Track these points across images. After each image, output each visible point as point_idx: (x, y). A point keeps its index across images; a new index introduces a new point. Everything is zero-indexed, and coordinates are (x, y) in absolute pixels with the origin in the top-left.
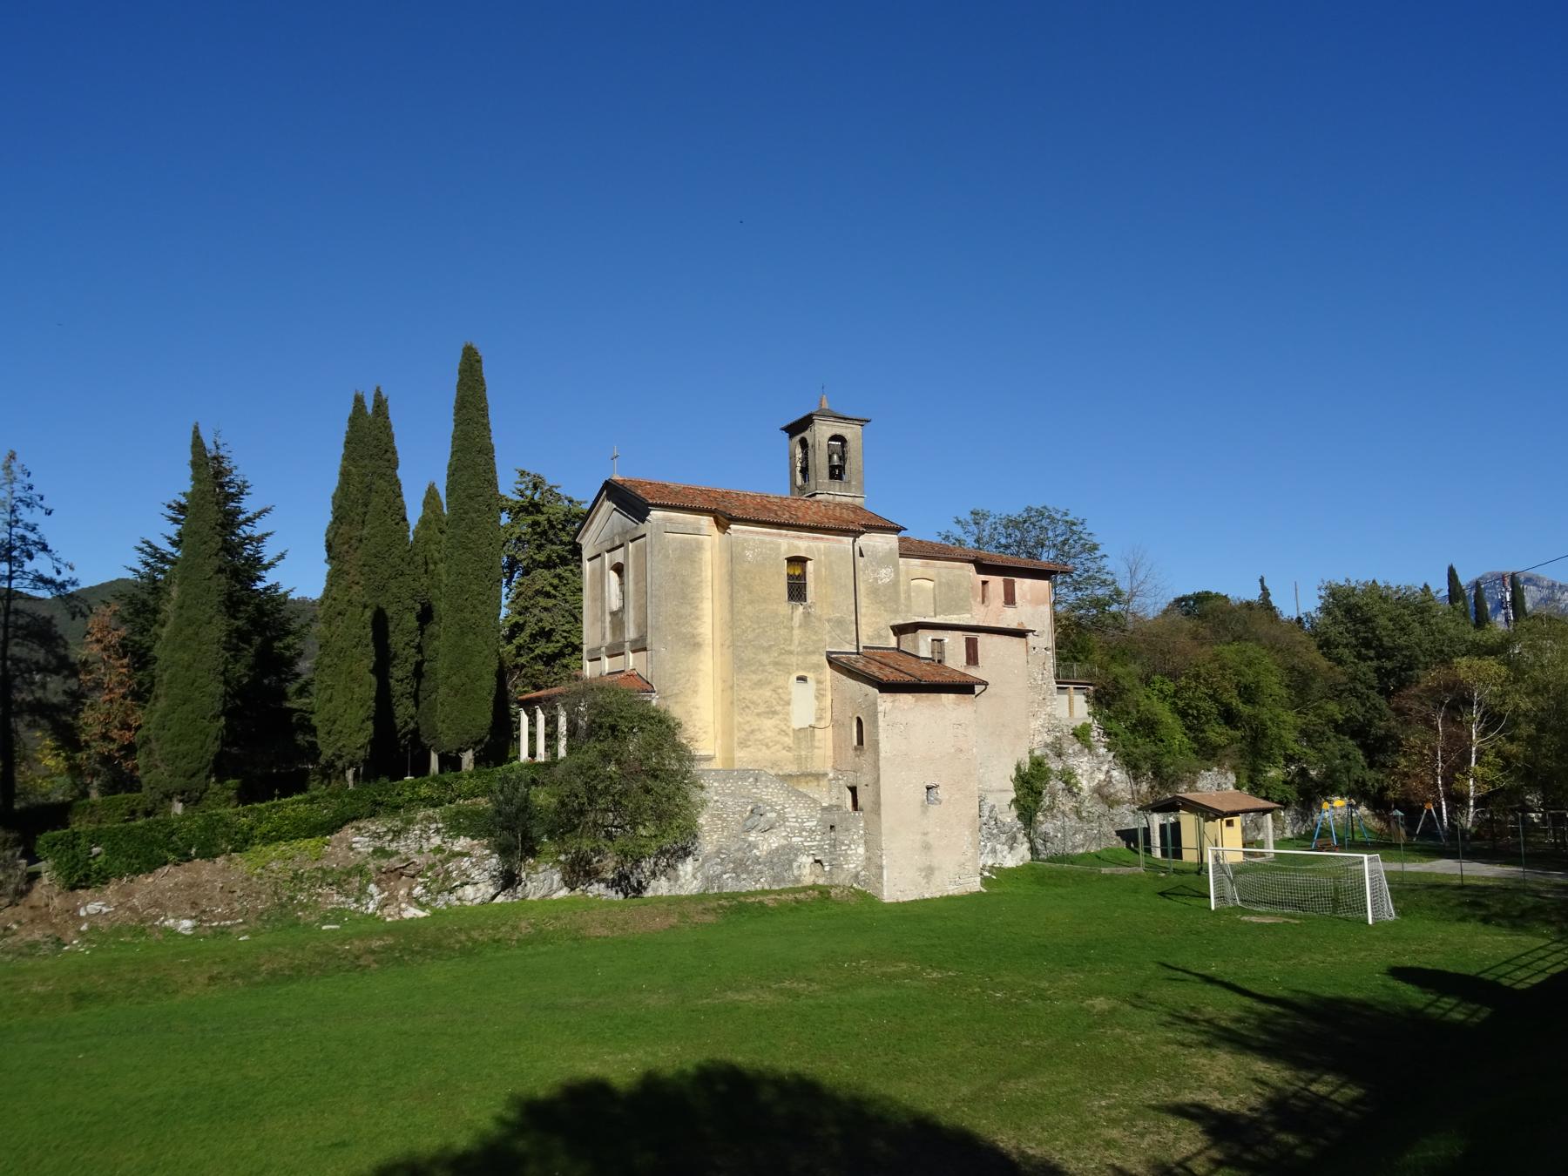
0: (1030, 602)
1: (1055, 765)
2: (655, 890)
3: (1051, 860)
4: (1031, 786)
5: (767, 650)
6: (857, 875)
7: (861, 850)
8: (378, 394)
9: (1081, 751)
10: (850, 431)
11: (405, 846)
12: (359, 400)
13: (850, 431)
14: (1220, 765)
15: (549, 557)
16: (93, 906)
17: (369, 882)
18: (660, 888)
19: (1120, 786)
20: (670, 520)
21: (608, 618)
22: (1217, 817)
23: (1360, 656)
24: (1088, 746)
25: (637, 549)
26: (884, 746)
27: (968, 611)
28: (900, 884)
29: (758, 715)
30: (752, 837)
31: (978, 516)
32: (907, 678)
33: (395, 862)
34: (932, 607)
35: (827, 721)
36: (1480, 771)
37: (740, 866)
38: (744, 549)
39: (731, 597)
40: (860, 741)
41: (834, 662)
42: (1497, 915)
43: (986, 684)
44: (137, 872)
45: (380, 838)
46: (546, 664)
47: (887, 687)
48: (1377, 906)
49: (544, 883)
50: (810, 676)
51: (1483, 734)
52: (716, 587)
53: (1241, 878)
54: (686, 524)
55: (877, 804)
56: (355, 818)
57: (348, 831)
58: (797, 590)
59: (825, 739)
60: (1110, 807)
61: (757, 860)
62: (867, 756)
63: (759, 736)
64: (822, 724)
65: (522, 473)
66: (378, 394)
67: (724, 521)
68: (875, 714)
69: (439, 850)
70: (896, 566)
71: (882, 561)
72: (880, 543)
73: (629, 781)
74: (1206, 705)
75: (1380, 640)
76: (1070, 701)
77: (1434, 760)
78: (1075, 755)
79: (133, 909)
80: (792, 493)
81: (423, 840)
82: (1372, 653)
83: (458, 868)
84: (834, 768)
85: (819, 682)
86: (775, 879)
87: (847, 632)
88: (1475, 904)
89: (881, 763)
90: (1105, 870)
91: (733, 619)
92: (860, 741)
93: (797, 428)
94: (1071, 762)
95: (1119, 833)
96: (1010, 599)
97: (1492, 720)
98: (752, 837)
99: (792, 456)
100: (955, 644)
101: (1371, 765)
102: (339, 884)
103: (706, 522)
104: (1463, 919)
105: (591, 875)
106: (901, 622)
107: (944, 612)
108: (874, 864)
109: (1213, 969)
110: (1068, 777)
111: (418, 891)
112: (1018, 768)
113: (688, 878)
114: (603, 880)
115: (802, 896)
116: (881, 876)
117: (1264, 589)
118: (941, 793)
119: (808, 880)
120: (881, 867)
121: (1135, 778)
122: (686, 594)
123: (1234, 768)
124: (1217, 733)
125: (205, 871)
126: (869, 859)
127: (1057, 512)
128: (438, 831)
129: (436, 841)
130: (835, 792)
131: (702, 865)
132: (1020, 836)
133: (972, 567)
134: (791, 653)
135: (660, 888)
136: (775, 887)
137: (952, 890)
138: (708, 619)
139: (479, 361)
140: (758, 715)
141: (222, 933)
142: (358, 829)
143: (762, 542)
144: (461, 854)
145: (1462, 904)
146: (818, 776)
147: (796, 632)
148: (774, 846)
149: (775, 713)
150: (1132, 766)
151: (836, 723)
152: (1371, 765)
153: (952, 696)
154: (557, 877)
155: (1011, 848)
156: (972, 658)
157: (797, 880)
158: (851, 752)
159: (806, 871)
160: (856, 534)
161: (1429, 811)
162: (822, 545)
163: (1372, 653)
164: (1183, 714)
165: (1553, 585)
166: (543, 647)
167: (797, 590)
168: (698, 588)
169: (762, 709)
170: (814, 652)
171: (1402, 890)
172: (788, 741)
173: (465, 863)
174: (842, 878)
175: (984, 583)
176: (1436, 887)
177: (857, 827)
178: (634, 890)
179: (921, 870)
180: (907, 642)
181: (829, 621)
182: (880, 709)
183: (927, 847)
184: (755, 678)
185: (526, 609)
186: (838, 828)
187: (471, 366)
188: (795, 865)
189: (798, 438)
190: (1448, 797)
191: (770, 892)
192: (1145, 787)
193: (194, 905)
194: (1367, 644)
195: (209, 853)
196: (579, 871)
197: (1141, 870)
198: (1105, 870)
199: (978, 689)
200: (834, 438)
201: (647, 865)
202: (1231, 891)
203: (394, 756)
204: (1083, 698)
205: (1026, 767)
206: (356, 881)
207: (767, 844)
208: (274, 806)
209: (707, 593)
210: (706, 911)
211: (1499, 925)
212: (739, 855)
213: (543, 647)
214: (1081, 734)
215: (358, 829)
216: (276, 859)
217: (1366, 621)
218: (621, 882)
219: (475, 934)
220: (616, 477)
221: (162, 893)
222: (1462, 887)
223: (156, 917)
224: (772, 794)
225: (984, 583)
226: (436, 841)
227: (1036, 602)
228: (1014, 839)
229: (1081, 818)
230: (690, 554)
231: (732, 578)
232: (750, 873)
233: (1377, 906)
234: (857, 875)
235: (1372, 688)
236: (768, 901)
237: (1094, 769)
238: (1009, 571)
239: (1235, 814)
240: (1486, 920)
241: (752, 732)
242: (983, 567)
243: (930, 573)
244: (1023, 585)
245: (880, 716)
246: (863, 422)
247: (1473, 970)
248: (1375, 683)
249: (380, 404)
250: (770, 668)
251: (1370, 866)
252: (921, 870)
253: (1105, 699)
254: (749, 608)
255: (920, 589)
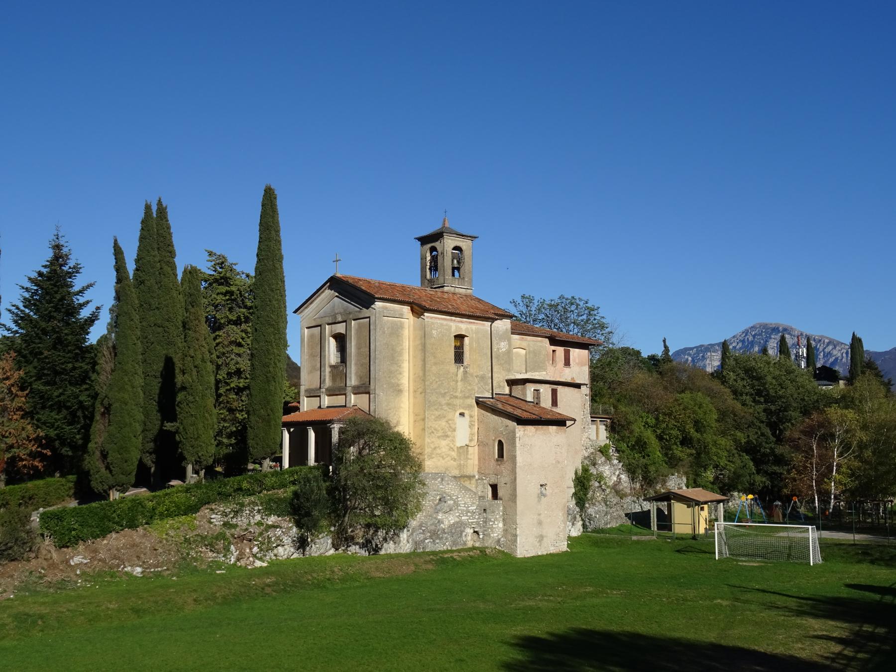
0: (578, 364)
1: (593, 471)
2: (386, 550)
3: (594, 531)
4: (582, 483)
5: (444, 395)
6: (499, 541)
7: (501, 525)
8: (160, 203)
9: (605, 462)
10: (464, 244)
11: (241, 521)
12: (148, 208)
13: (464, 244)
14: (678, 472)
15: (239, 317)
16: (78, 558)
17: (230, 543)
18: (389, 548)
19: (625, 485)
20: (386, 308)
21: (328, 370)
22: (696, 505)
23: (754, 401)
24: (608, 458)
25: (360, 327)
26: (519, 459)
27: (545, 370)
28: (526, 547)
29: (439, 437)
30: (440, 516)
31: (528, 300)
32: (534, 417)
33: (237, 532)
34: (524, 367)
35: (475, 442)
36: (838, 477)
37: (435, 535)
38: (432, 329)
39: (424, 360)
40: (501, 455)
41: (480, 403)
42: (877, 559)
43: (575, 420)
44: (95, 537)
45: (226, 516)
46: (237, 394)
47: (522, 422)
48: (814, 557)
49: (323, 546)
50: (467, 412)
51: (840, 455)
52: (411, 353)
53: (731, 541)
54: (394, 311)
55: (513, 497)
56: (208, 503)
57: (205, 511)
58: (459, 357)
59: (474, 452)
60: (621, 498)
61: (444, 531)
62: (505, 468)
63: (438, 451)
64: (472, 444)
65: (211, 254)
66: (160, 203)
67: (418, 310)
68: (514, 438)
69: (259, 524)
70: (509, 340)
71: (502, 338)
72: (503, 325)
73: (352, 479)
74: (675, 432)
75: (768, 391)
76: (597, 429)
77: (812, 471)
78: (603, 464)
79: (102, 560)
80: (422, 283)
81: (251, 518)
82: (762, 400)
83: (275, 535)
84: (479, 472)
85: (471, 416)
86: (454, 543)
87: (486, 384)
88: (865, 554)
89: (518, 470)
90: (634, 538)
91: (422, 377)
92: (501, 455)
93: (430, 240)
94: (601, 469)
95: (627, 515)
96: (567, 363)
97: (846, 447)
98: (440, 516)
99: (423, 258)
100: (545, 391)
101: (758, 472)
102: (212, 547)
103: (406, 309)
104: (859, 562)
105: (351, 540)
106: (513, 377)
107: (534, 370)
108: (511, 533)
109: (765, 587)
110: (600, 478)
111: (255, 550)
112: (576, 473)
113: (404, 543)
114: (357, 544)
115: (471, 553)
116: (516, 541)
117: (666, 347)
118: (548, 491)
119: (470, 544)
120: (516, 536)
121: (633, 480)
122: (394, 357)
123: (686, 473)
124: (678, 451)
125: (136, 535)
126: (505, 531)
127: (580, 300)
128: (259, 511)
129: (258, 517)
130: (480, 488)
131: (412, 534)
132: (578, 516)
133: (547, 341)
134: (456, 397)
135: (389, 548)
136: (454, 548)
137: (552, 550)
138: (406, 374)
139: (275, 198)
140: (439, 437)
141: (158, 575)
142: (212, 510)
143: (442, 324)
144: (274, 527)
145: (857, 554)
146: (470, 477)
147: (459, 384)
148: (452, 522)
149: (447, 436)
150: (631, 471)
151: (481, 444)
152: (758, 472)
153: (554, 427)
154: (330, 541)
155: (573, 524)
156: (555, 403)
157: (465, 544)
158: (493, 463)
159: (469, 538)
160: (492, 320)
161: (795, 502)
162: (474, 327)
163: (762, 400)
164: (660, 438)
165: (802, 334)
166: (235, 383)
167: (459, 357)
168: (401, 354)
169: (440, 434)
170: (468, 397)
171: (825, 546)
172: (454, 454)
173: (278, 532)
174: (489, 543)
175: (554, 351)
176: (839, 545)
177: (499, 510)
178: (374, 550)
179: (537, 537)
180: (517, 391)
181: (477, 376)
182: (517, 435)
183: (540, 523)
184: (437, 413)
185: (224, 354)
186: (488, 511)
187: (269, 199)
188: (464, 534)
189: (429, 245)
190: (819, 493)
191: (452, 551)
192: (638, 485)
193: (138, 557)
194: (759, 393)
195: (133, 525)
196: (342, 539)
197: (654, 537)
198: (634, 538)
199: (568, 423)
200: (456, 248)
201: (381, 533)
202: (726, 550)
203: (235, 462)
204: (604, 427)
205: (580, 472)
206: (220, 545)
207: (448, 520)
208: (167, 494)
209: (406, 356)
210: (426, 562)
211: (879, 565)
212: (433, 527)
213: (235, 383)
214: (603, 451)
215: (212, 510)
216: (169, 530)
217: (759, 378)
218: (367, 544)
219: (315, 575)
220: (339, 275)
221: (118, 550)
222: (854, 545)
223: (118, 566)
224: (450, 488)
225: (554, 351)
226: (258, 517)
227: (581, 364)
228: (575, 518)
229: (606, 505)
230: (396, 331)
231: (424, 348)
232: (441, 539)
233: (814, 557)
234: (499, 541)
235: (762, 422)
236: (455, 555)
237: (612, 472)
238: (568, 344)
239: (706, 503)
240: (872, 562)
241: (435, 448)
242: (554, 341)
243: (524, 344)
244: (575, 353)
245: (517, 440)
246: (473, 238)
247: (887, 585)
248: (764, 419)
249: (162, 211)
250: (445, 408)
251: (812, 534)
252: (537, 537)
253: (613, 429)
254: (434, 368)
255: (518, 355)
